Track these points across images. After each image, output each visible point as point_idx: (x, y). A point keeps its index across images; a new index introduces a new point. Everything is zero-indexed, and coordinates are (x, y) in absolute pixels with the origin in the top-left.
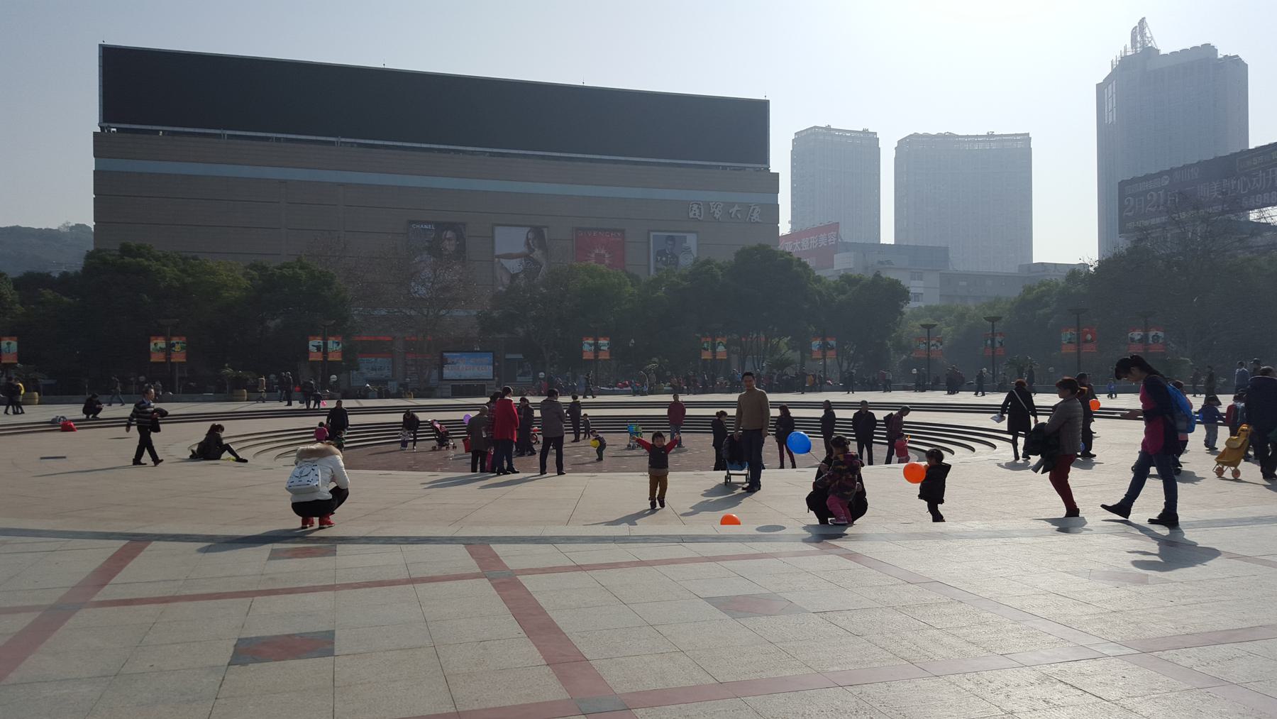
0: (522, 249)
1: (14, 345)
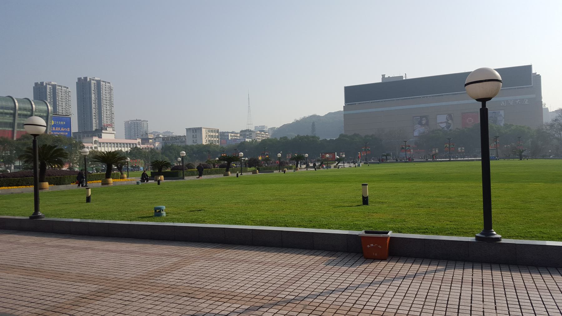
0: (445, 120)
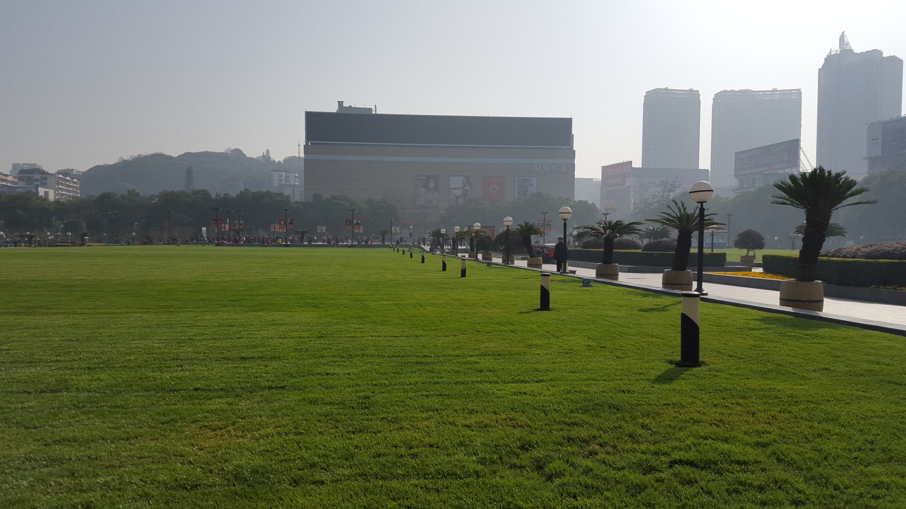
1: (325, 228)
